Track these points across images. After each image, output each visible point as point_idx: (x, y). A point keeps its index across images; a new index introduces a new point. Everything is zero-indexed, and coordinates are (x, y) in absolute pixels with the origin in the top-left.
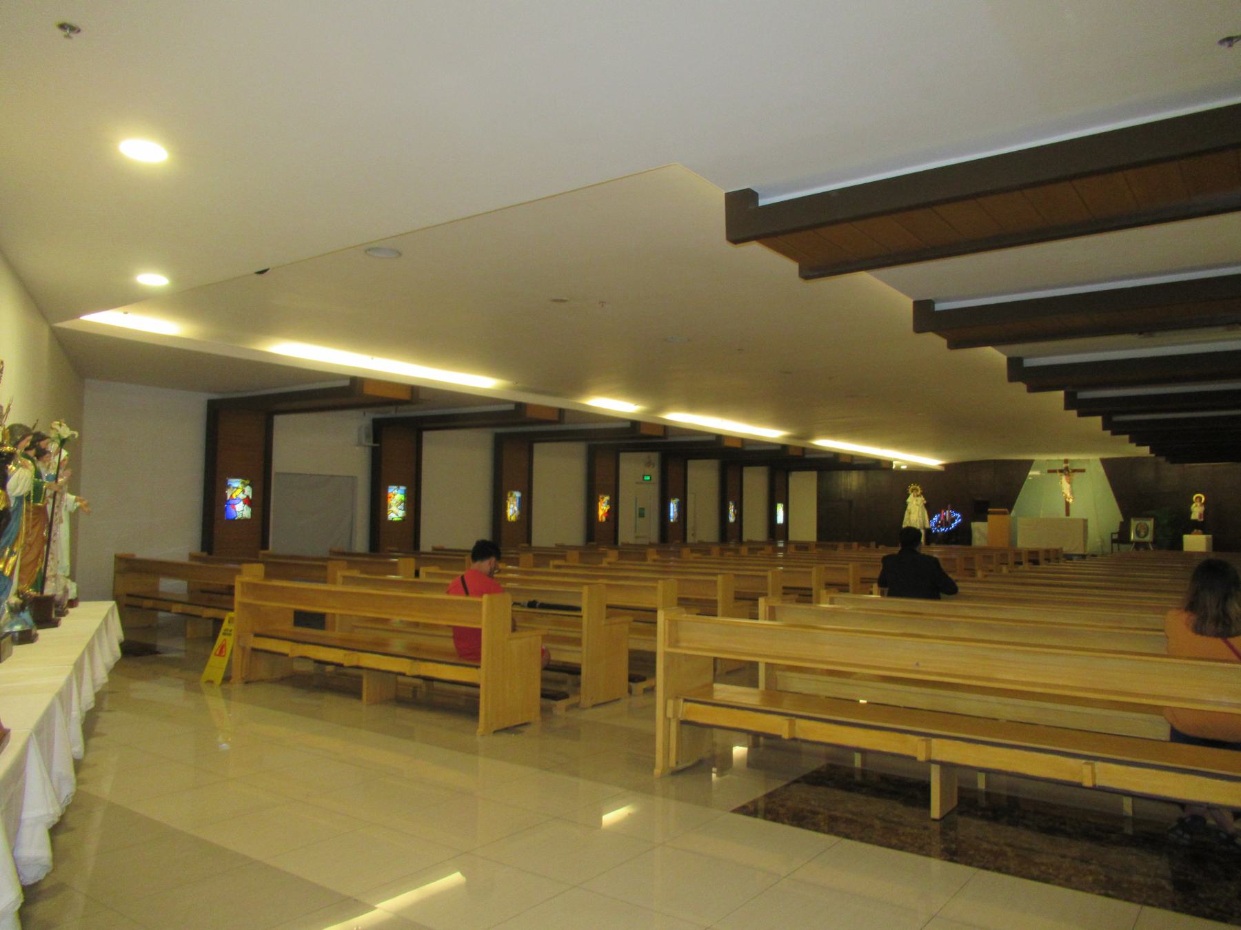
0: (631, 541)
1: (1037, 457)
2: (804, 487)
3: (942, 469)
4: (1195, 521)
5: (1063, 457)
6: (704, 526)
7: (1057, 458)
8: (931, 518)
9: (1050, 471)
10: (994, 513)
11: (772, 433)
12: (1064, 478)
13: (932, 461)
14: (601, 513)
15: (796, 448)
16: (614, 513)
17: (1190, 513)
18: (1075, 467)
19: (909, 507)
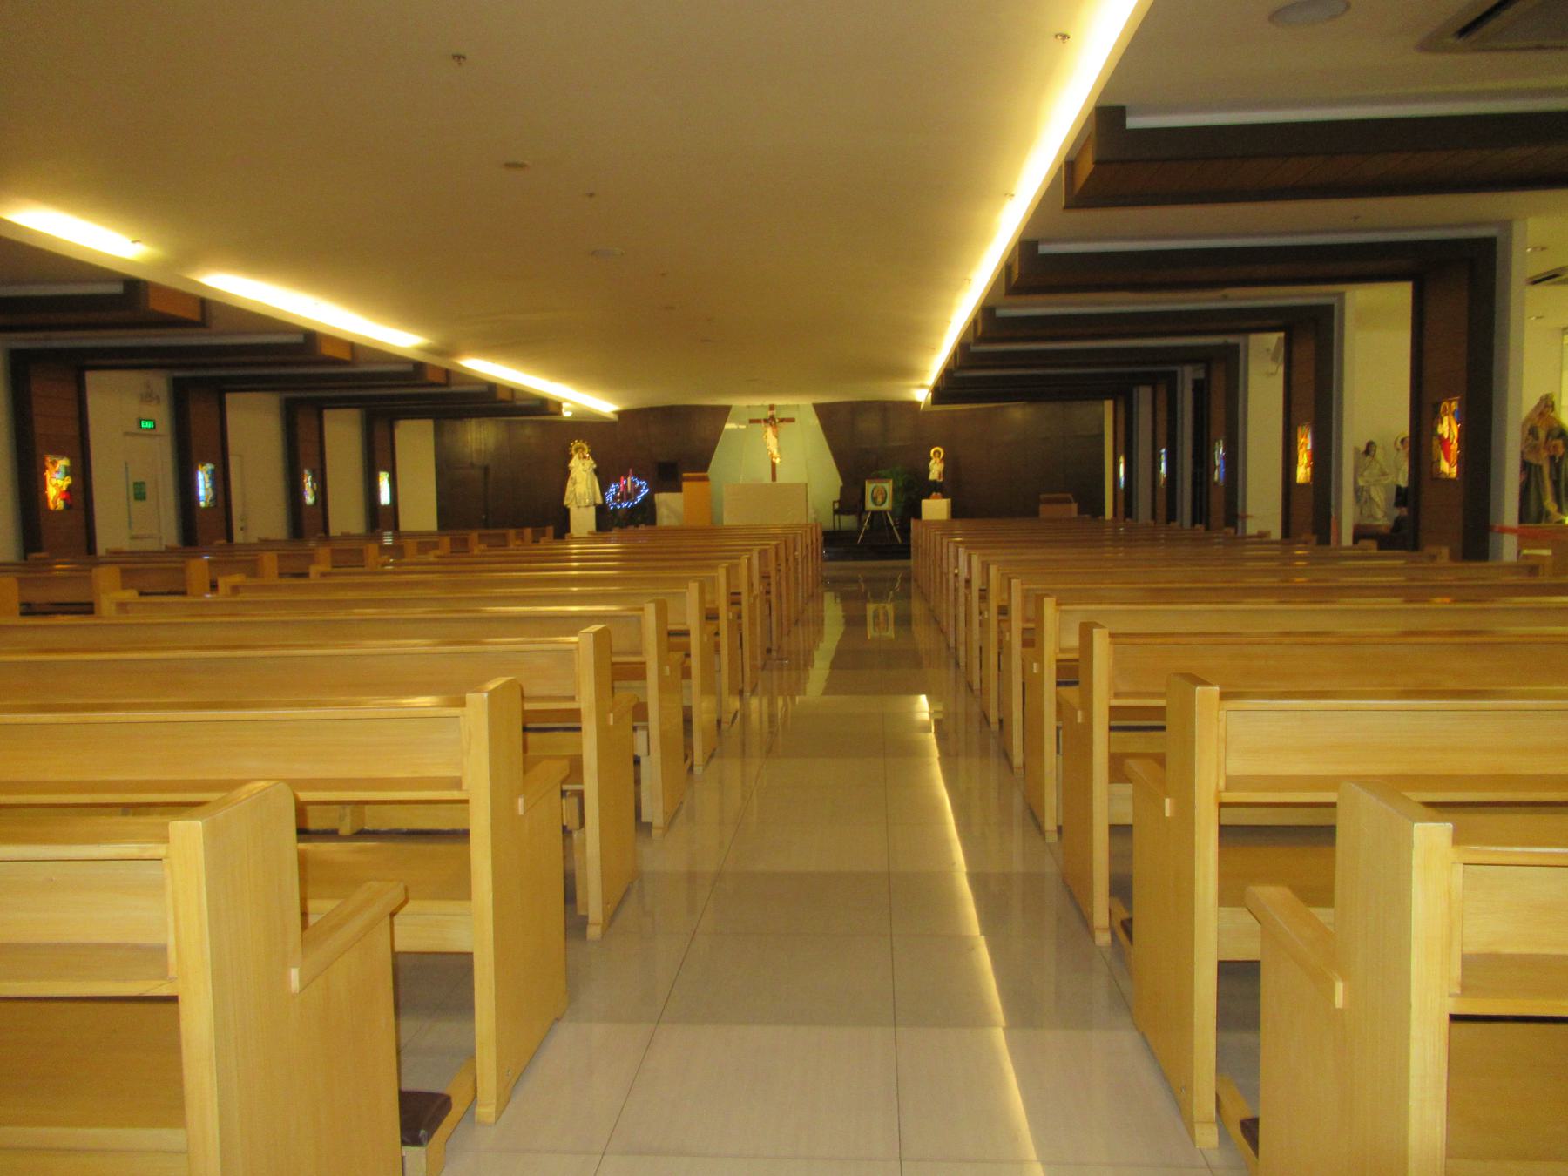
0: (126, 545)
1: (738, 402)
2: (415, 442)
3: (614, 417)
4: (935, 482)
5: (768, 402)
6: (260, 512)
8: (604, 489)
9: (752, 421)
10: (689, 479)
11: (402, 339)
12: (770, 430)
13: (603, 405)
14: (202, 493)
15: (435, 368)
16: (81, 492)
17: (928, 471)
18: (782, 416)
19: (573, 475)
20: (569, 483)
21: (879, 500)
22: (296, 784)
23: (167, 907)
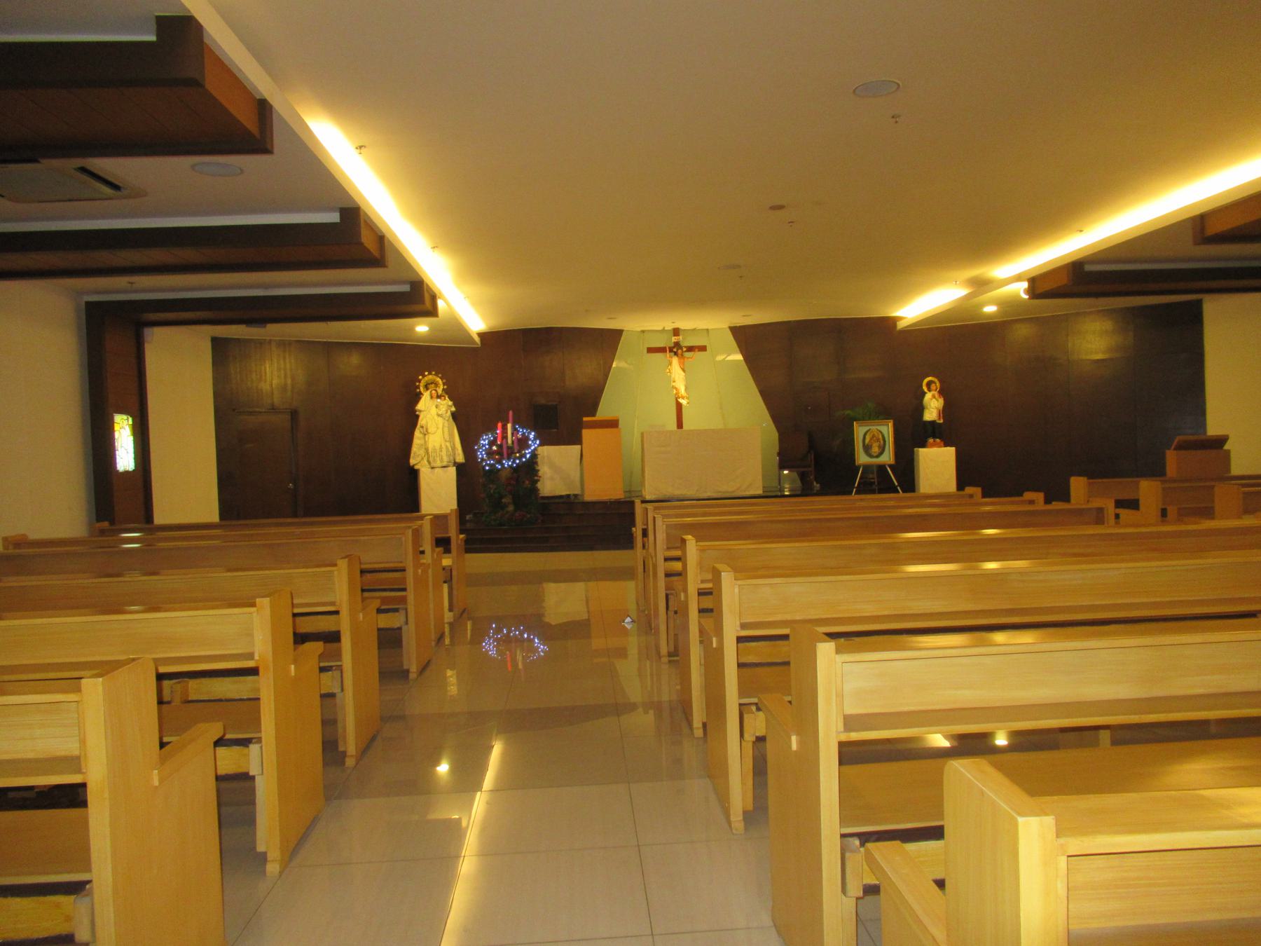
4: (933, 423)
5: (669, 326)
7: (658, 323)
8: (468, 442)
12: (675, 360)
17: (920, 408)
19: (422, 421)
20: (417, 434)
21: (875, 450)
22: (156, 661)
23: (85, 729)
